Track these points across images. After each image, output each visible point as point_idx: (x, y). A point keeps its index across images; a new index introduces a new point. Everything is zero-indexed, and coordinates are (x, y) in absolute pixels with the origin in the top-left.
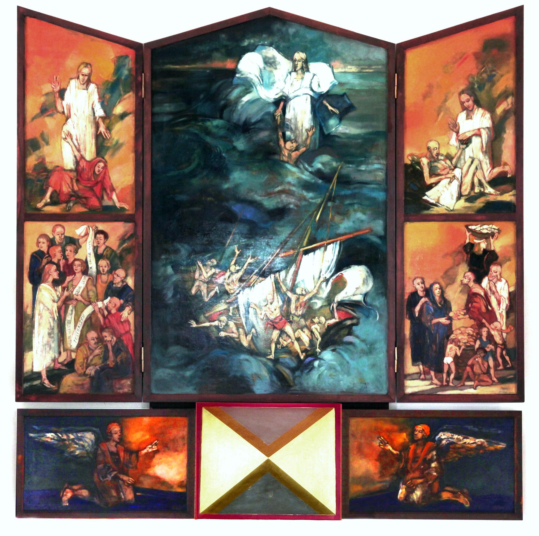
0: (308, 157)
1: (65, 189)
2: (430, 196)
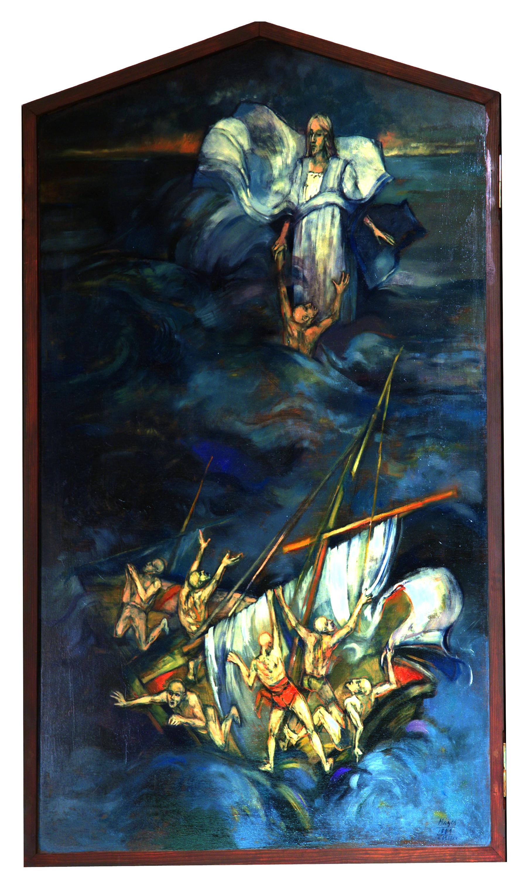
0: (335, 339)
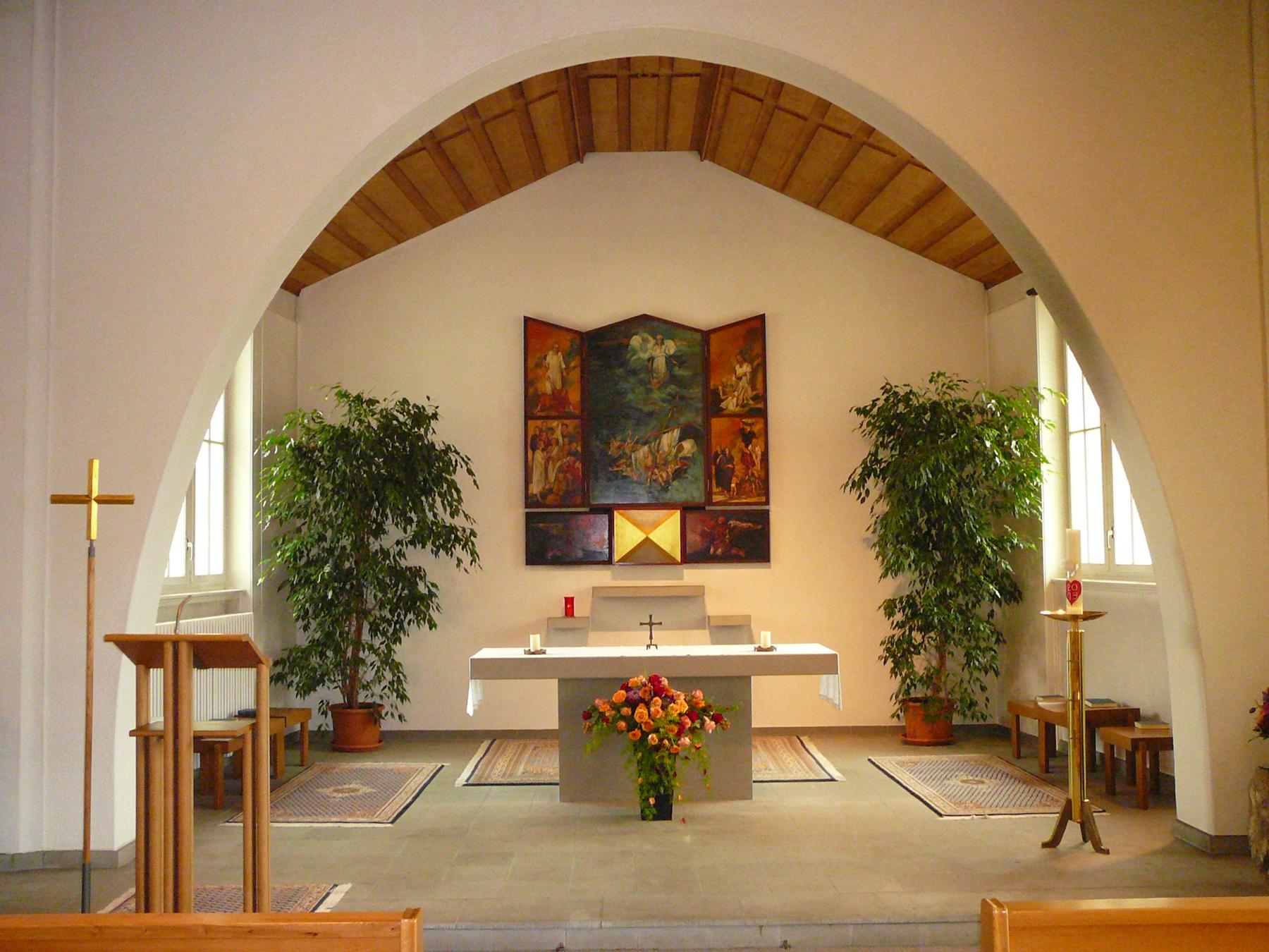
0: (663, 385)
1: (547, 404)
2: (723, 405)
